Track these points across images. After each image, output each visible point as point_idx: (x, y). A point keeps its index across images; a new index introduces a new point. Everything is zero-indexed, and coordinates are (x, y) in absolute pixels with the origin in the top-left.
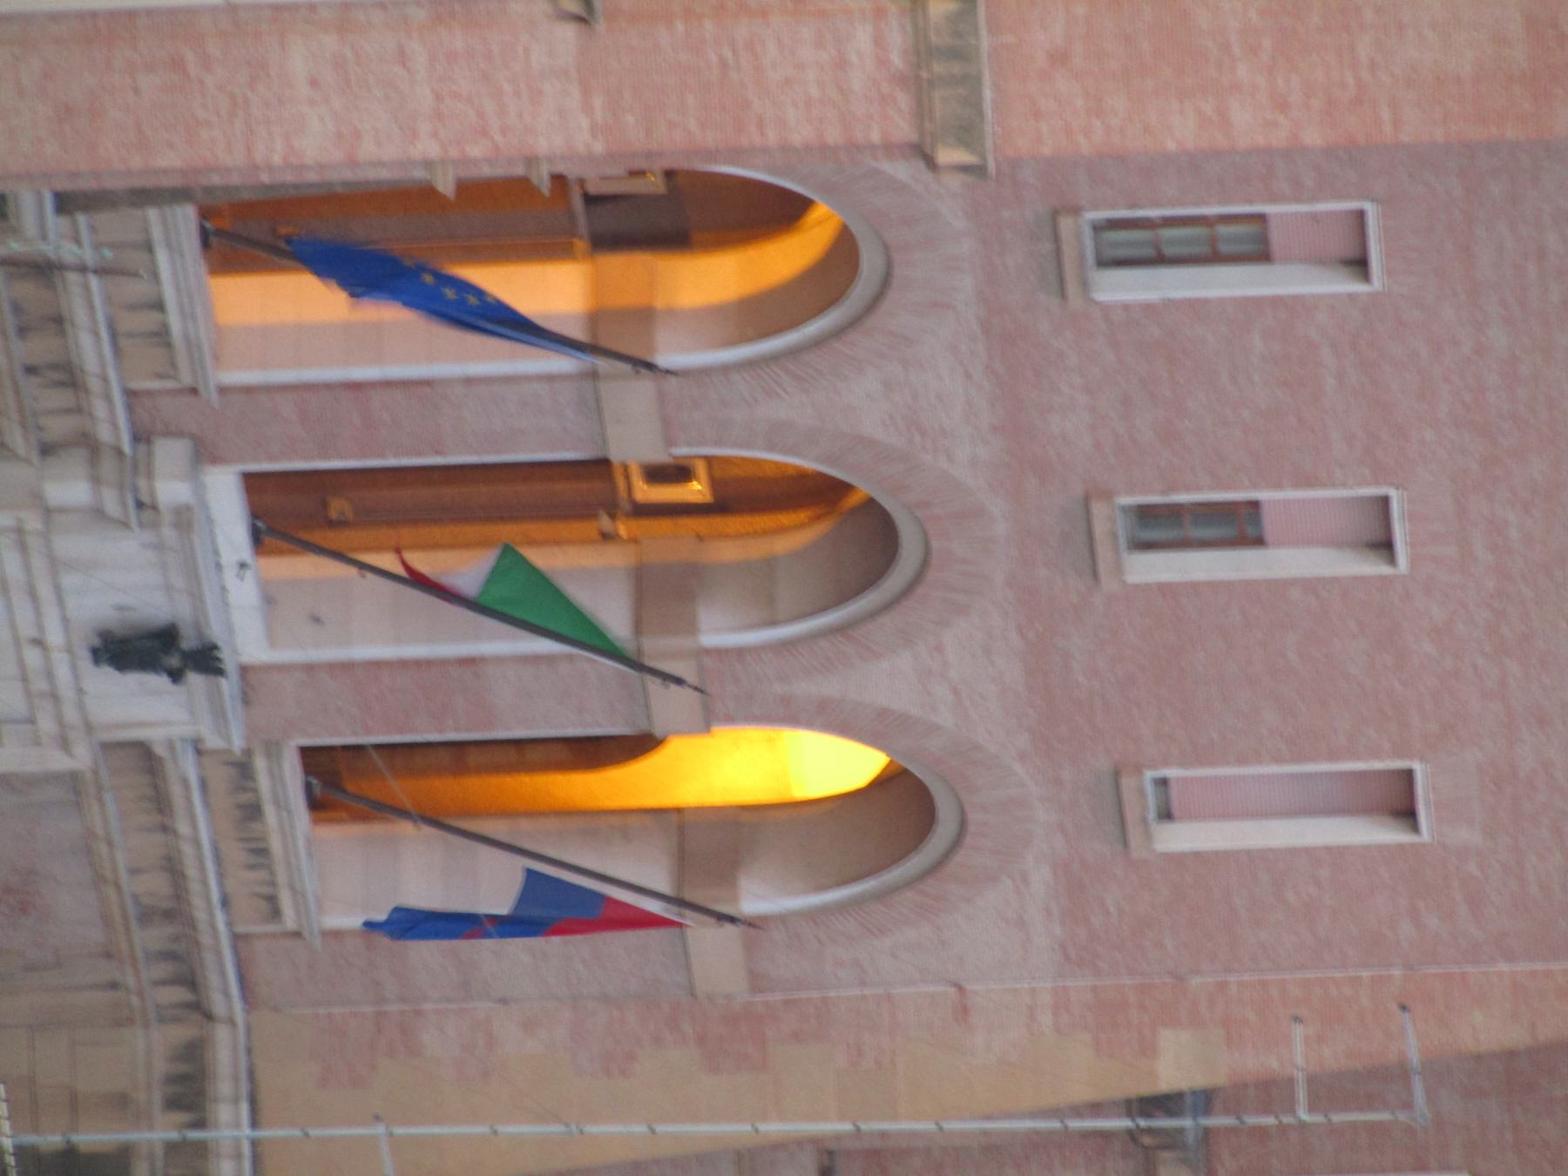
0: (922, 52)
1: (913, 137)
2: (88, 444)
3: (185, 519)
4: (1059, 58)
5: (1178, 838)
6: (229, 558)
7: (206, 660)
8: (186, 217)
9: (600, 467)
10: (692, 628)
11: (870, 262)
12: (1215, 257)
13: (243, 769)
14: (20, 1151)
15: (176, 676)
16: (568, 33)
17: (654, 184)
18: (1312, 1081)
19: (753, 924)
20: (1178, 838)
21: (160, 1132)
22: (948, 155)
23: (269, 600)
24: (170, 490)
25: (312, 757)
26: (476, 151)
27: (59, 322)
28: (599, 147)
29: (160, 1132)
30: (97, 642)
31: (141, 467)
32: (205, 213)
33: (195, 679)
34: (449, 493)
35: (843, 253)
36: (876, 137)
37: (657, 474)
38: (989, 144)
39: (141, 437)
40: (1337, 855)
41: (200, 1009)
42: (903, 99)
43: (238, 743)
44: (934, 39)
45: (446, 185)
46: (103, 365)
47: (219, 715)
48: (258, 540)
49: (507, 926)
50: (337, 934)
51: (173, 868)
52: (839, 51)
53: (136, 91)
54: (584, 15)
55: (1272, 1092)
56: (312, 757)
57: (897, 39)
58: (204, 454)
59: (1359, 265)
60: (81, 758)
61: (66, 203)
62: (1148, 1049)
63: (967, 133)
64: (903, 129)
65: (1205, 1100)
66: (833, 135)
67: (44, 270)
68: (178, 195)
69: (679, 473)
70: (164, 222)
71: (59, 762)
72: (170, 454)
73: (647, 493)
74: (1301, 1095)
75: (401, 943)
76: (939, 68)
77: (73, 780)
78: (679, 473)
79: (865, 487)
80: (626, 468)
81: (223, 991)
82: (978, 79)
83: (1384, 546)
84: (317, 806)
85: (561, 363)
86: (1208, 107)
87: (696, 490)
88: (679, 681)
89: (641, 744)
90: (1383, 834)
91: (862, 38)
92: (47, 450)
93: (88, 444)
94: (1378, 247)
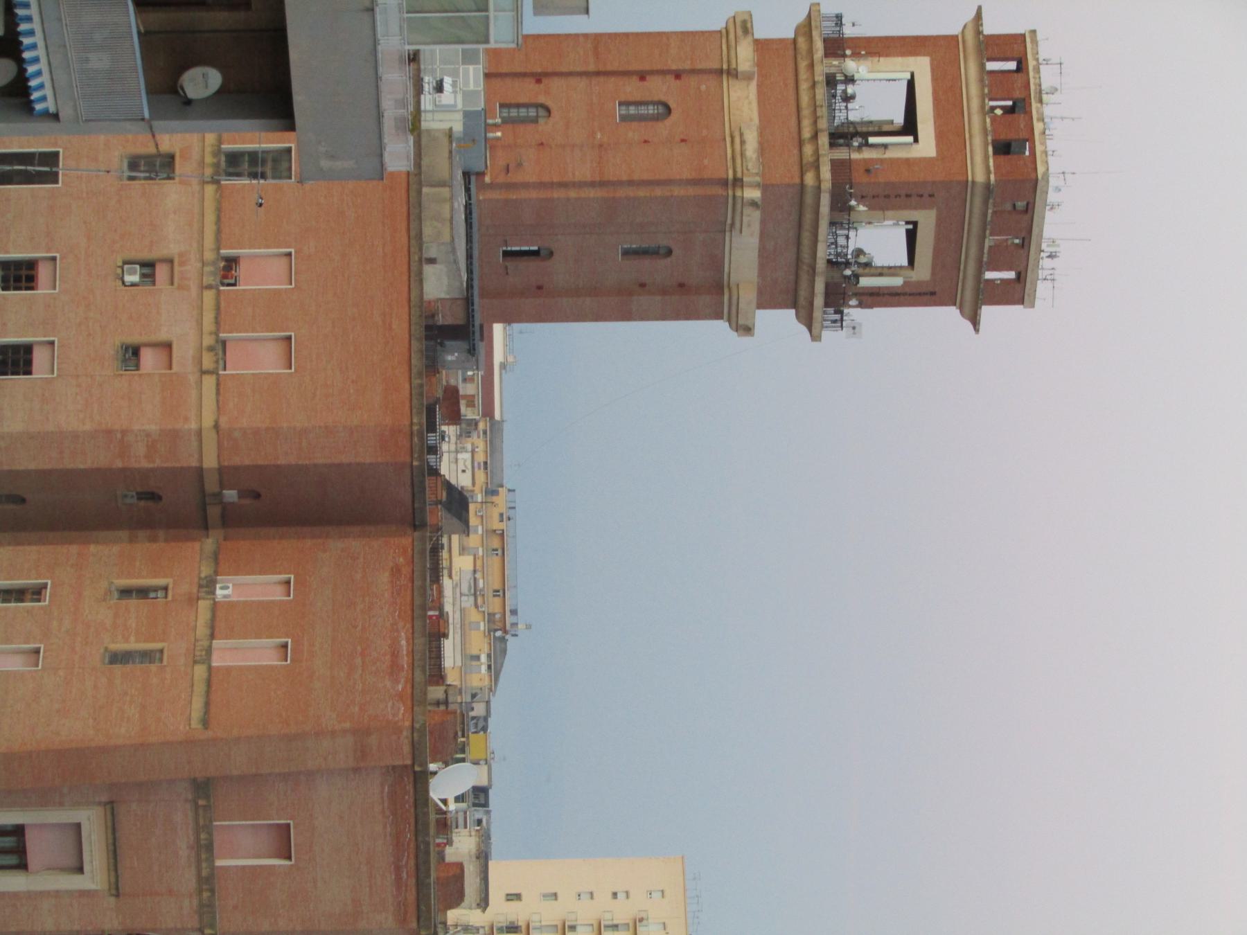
0: (201, 905)
1: (199, 926)
4: (235, 907)
16: (112, 899)
18: (506, 927)
26: (89, 928)
28: (120, 928)
34: (443, 109)
36: (189, 926)
38: (218, 929)
42: (196, 917)
44: (204, 902)
52: (597, 58)
53: (4, 912)
57: (195, 902)
63: (212, 926)
64: (197, 926)
66: (179, 926)
76: (205, 909)
82: (216, 912)
86: (273, 920)
91: (186, 903)
94: (488, 744)
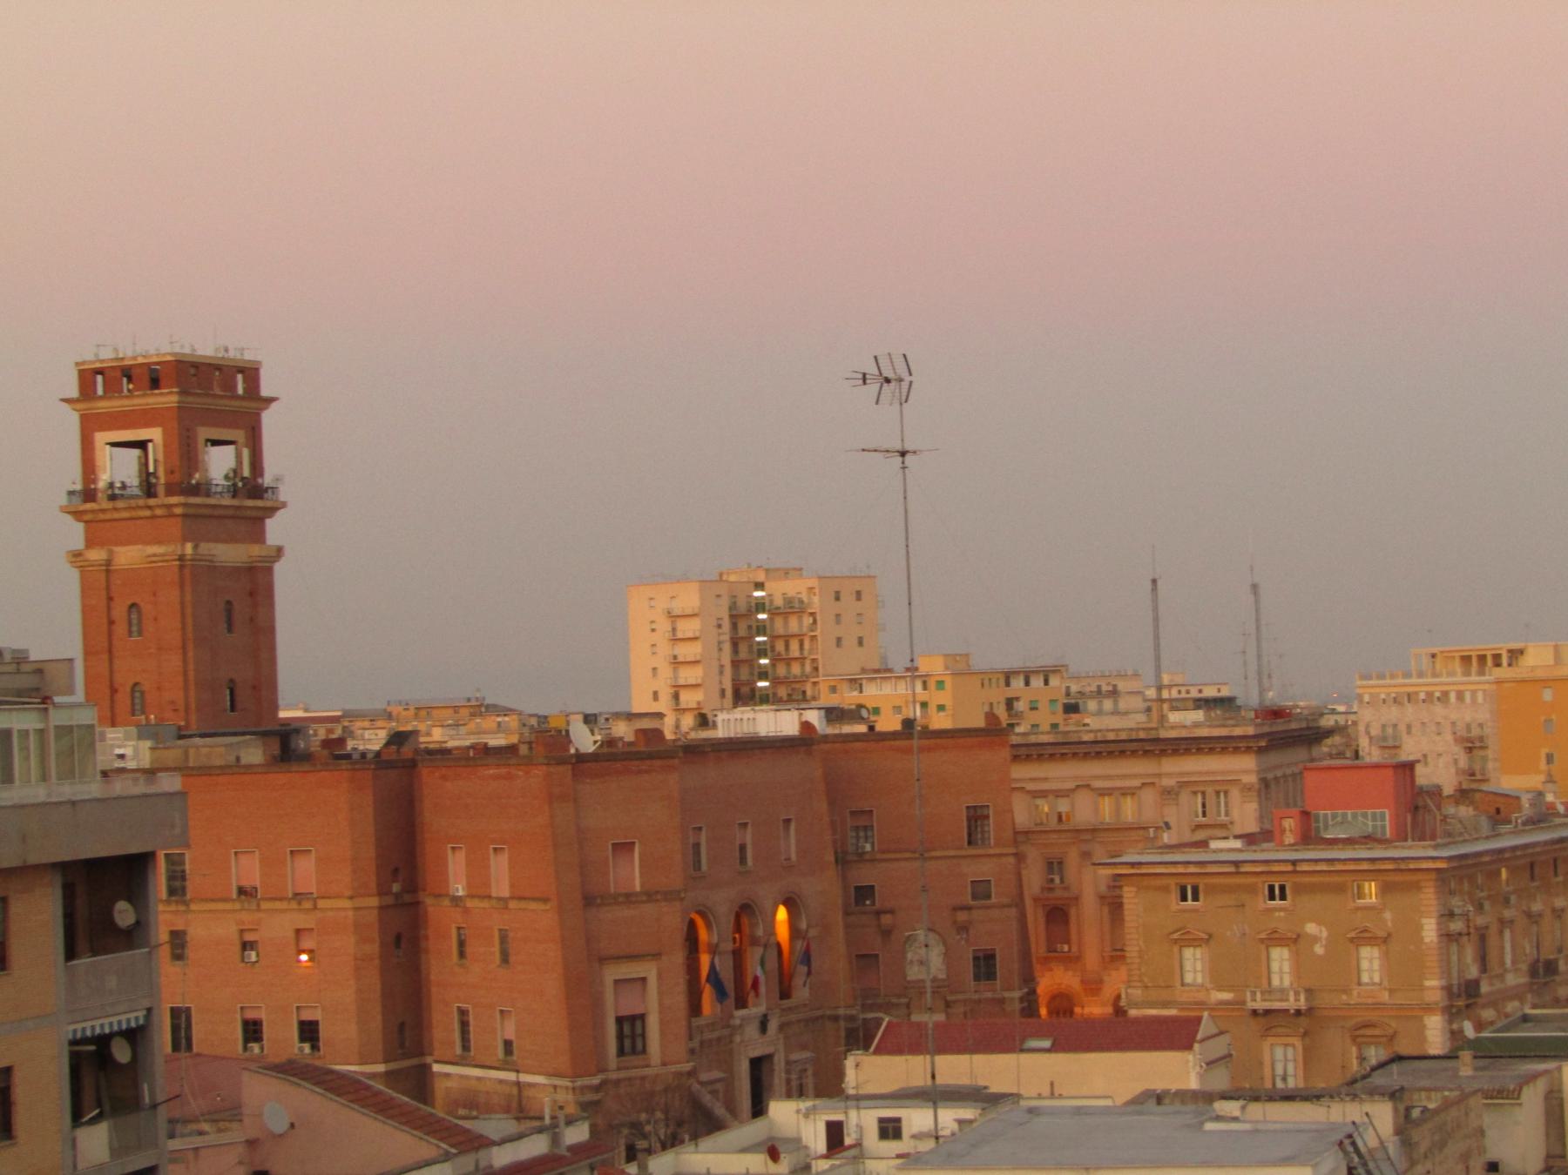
2: (731, 1035)
3: (743, 1019)
5: (794, 857)
6: (748, 1012)
8: (693, 1020)
10: (760, 937)
11: (701, 908)
13: (783, 1010)
14: (846, 1046)
15: (768, 1020)
17: (687, 943)
20: (794, 857)
21: (842, 1024)
24: (737, 1022)
29: (842, 1024)
30: (1486, 1167)
32: (693, 1017)
33: (769, 1018)
35: (699, 913)
37: (735, 942)
39: (729, 1026)
41: (822, 1017)
45: (687, 977)
48: (746, 1007)
49: (809, 967)
50: (722, 1011)
57: (663, 904)
60: (781, 1036)
61: (691, 1038)
65: (836, 853)
67: (702, 1043)
68: (690, 1023)
69: (734, 939)
70: (926, 1081)
71: (781, 1041)
72: (732, 1022)
73: (737, 945)
74: (915, 750)
78: (734, 939)
79: (737, 909)
80: (998, 687)
81: (819, 1013)
87: (737, 936)
89: (779, 945)
90: (793, 826)
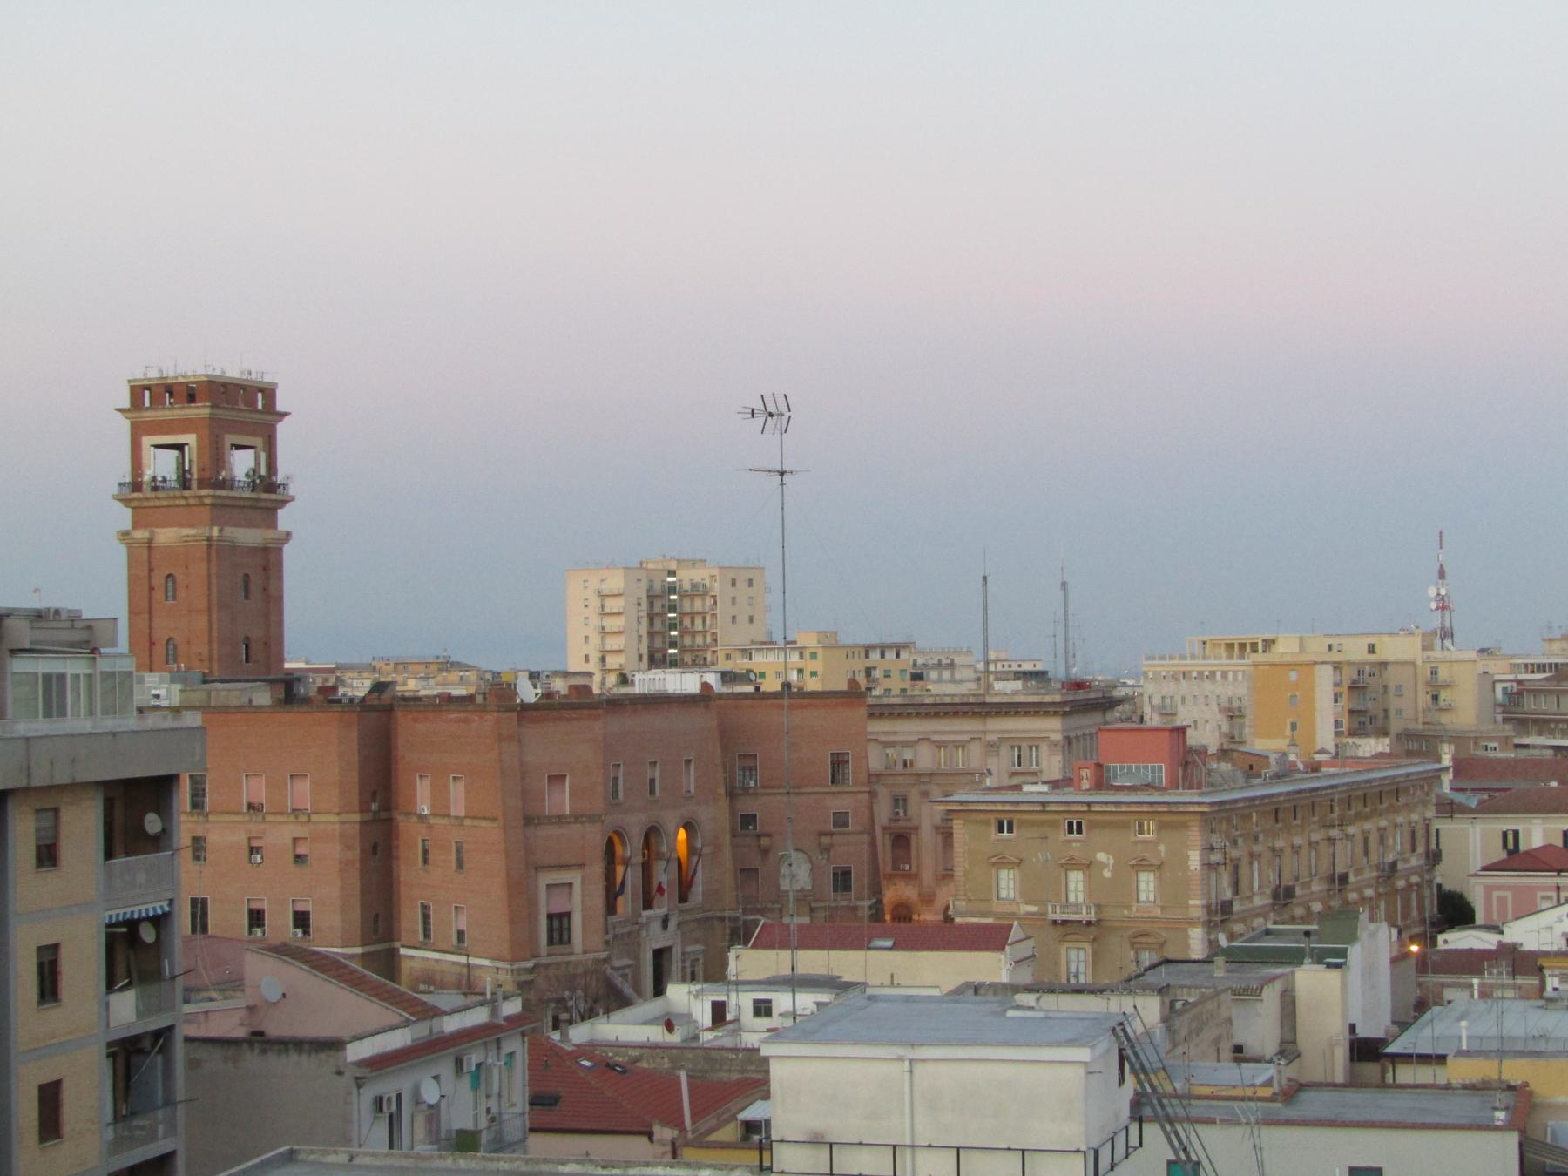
2: (639, 930)
3: (648, 918)
5: (692, 790)
7: (667, 916)
9: (643, 864)
12: (618, 784)
13: (682, 911)
19: (702, 845)
20: (692, 790)
22: (603, 818)
23: (659, 907)
25: (680, 902)
27: (622, 935)
31: (641, 923)
35: (617, 833)
37: (644, 857)
39: (637, 923)
40: (695, 768)
43: (677, 912)
46: (1188, 1137)
47: (674, 914)
51: (693, 921)
54: (359, 1081)
55: (725, 778)
56: (680, 902)
58: (640, 916)
59: (619, 765)
60: (679, 933)
61: (607, 933)
62: (720, 795)
63: (600, 816)
64: (600, 824)
68: (606, 920)
72: (640, 920)
73: (646, 858)
75: (1546, 843)
77: (682, 933)
78: (644, 854)
81: (709, 914)
83: (655, 763)
84: (686, 901)
85: (629, 868)
87: (646, 852)
88: (1204, 652)
89: (679, 859)
90: (693, 764)
92: (639, 936)
93: (639, 930)
